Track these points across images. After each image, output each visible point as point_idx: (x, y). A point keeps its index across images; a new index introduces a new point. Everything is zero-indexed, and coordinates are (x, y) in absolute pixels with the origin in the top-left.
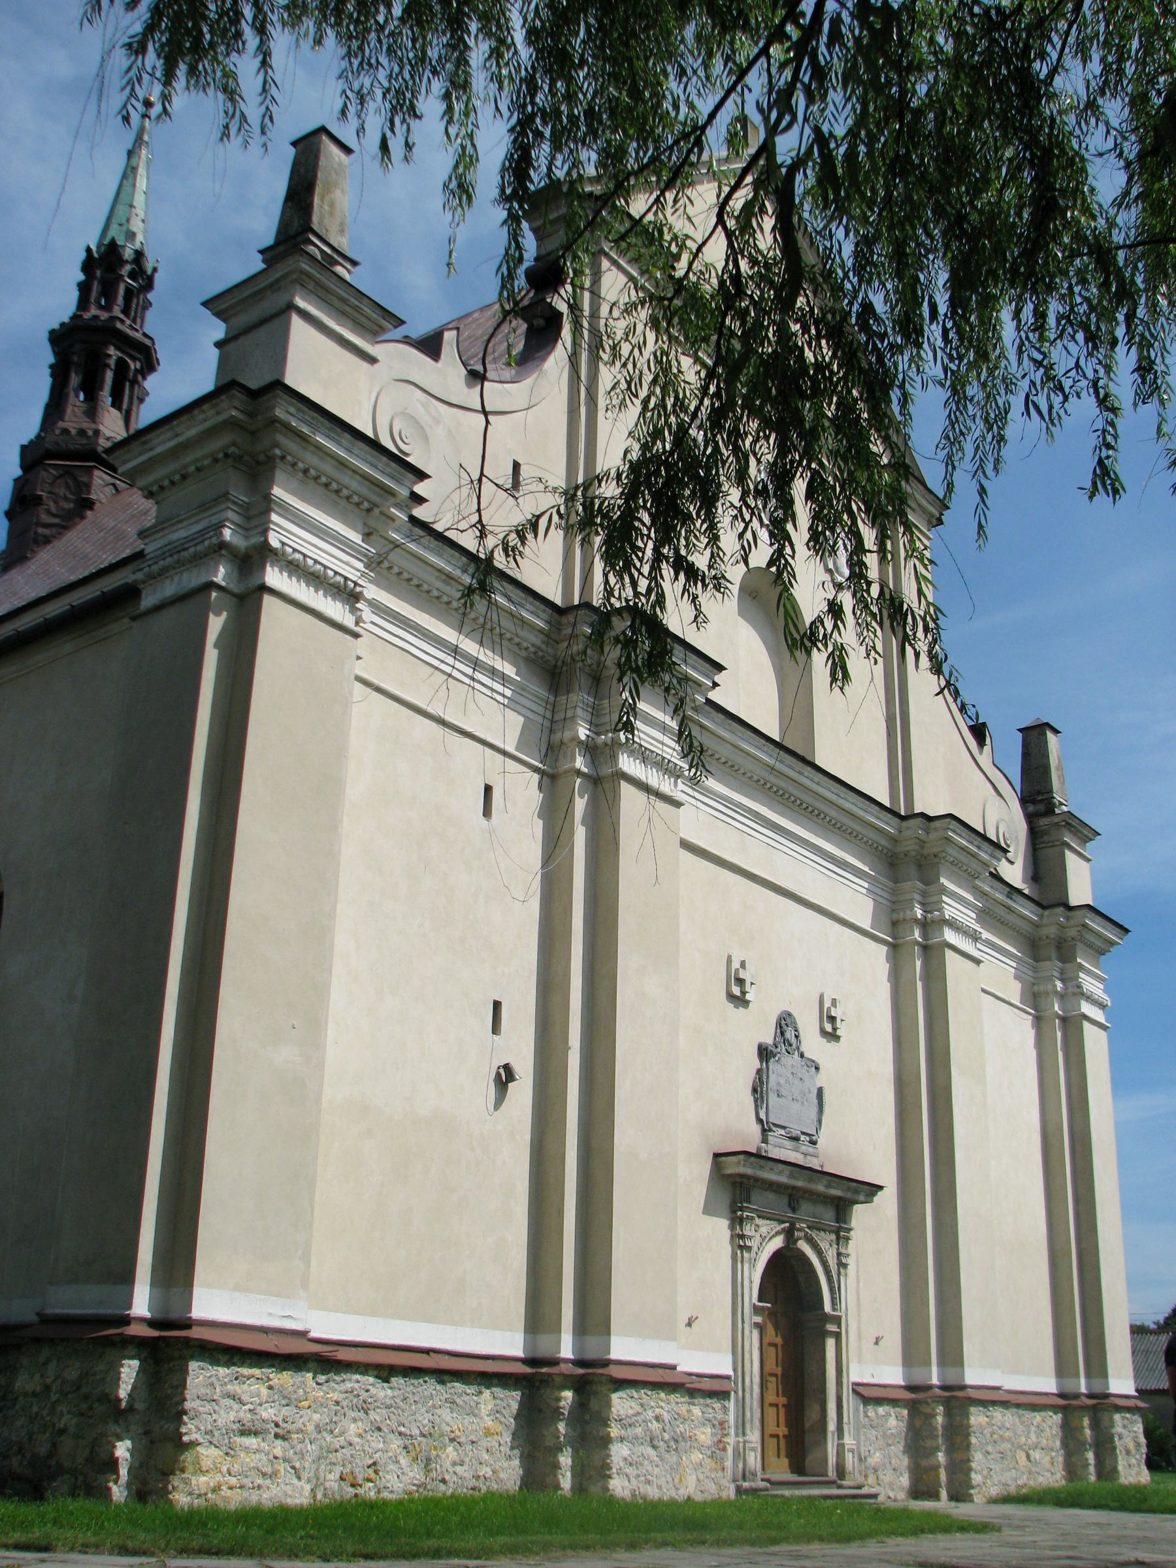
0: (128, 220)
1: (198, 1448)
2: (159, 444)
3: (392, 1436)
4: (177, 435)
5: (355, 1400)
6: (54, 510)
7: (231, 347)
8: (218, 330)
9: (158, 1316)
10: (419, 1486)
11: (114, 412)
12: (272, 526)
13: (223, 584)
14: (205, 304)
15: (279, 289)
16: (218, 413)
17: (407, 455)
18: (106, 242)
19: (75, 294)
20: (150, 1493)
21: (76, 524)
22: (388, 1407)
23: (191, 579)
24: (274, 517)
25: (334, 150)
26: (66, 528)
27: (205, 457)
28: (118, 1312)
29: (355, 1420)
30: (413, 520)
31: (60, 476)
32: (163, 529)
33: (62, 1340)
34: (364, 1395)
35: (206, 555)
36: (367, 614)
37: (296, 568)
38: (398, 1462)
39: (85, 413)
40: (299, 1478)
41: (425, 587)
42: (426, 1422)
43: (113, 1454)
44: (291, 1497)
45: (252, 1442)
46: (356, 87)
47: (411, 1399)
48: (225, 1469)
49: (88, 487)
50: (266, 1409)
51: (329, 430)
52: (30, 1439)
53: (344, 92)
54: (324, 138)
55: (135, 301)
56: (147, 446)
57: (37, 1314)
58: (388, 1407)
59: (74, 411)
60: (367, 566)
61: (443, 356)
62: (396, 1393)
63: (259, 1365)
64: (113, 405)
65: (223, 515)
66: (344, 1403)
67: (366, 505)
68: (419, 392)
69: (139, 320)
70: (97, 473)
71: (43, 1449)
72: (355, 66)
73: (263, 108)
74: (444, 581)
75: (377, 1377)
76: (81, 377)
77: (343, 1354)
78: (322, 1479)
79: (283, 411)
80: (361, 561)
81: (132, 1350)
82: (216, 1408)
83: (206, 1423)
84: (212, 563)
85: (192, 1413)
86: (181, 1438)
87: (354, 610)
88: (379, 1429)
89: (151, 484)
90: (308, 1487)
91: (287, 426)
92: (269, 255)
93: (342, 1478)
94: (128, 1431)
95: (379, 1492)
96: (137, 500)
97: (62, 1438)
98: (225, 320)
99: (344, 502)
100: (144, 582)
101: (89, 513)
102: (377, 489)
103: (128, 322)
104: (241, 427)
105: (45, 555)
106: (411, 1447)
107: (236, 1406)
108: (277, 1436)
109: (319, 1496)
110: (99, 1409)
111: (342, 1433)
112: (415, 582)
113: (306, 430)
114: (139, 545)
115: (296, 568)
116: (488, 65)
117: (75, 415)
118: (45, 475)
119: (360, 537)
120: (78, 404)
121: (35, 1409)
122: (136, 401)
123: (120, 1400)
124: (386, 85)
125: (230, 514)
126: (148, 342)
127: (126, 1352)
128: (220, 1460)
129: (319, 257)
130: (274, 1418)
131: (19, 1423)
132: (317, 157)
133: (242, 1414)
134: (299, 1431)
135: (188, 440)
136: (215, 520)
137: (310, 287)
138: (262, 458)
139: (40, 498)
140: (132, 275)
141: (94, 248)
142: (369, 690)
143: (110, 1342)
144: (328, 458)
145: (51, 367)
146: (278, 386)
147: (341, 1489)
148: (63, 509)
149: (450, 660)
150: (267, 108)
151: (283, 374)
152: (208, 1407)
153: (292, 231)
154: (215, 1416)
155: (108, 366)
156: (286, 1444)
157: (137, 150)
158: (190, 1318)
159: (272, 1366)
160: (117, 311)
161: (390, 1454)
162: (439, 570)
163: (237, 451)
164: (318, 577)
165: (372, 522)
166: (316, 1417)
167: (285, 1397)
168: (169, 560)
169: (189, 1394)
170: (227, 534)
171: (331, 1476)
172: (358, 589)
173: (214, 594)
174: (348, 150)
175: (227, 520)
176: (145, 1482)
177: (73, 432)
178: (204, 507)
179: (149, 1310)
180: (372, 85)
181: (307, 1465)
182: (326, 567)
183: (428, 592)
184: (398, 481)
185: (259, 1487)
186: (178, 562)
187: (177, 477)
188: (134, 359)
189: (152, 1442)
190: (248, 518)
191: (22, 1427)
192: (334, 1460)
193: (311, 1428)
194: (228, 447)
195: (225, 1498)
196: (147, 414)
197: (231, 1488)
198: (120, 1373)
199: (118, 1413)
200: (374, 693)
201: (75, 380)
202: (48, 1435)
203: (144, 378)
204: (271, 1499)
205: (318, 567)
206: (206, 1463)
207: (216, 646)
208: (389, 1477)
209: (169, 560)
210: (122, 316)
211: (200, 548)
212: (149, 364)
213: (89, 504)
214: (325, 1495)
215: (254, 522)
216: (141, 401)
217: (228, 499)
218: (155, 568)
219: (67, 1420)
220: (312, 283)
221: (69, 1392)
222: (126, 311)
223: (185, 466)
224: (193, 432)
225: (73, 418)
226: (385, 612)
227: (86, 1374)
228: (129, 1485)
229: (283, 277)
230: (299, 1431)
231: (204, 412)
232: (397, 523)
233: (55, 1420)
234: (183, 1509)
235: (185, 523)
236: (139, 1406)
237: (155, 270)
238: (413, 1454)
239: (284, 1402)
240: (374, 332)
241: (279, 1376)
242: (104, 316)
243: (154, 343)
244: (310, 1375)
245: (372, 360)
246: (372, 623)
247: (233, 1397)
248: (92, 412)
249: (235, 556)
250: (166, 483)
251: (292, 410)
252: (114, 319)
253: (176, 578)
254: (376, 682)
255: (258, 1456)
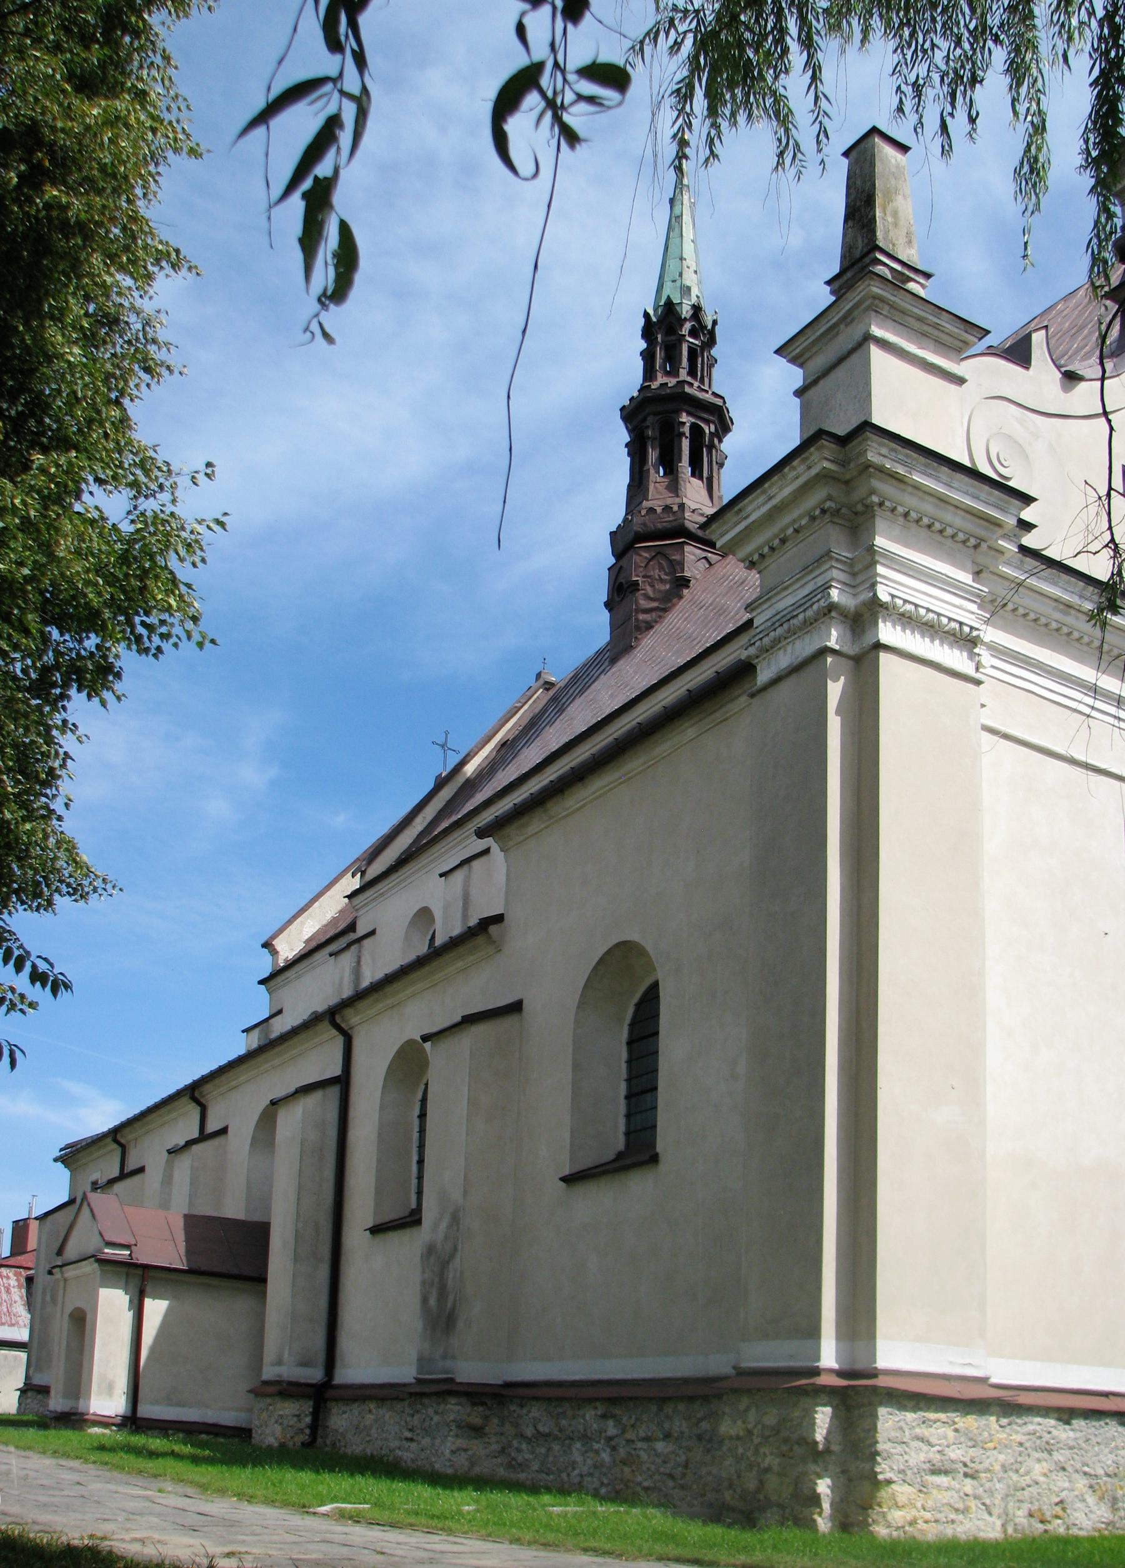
0: (681, 275)
1: (893, 1486)
2: (754, 510)
3: (1076, 1476)
4: (770, 498)
5: (1038, 1442)
6: (651, 595)
7: (810, 393)
8: (796, 376)
9: (846, 1367)
10: (1108, 1524)
11: (695, 482)
12: (879, 579)
13: (837, 647)
14: (778, 352)
15: (852, 321)
16: (810, 468)
17: (1008, 479)
18: (662, 303)
19: (639, 364)
20: (852, 1525)
21: (674, 605)
22: (1071, 1448)
23: (804, 647)
24: (880, 569)
25: (888, 151)
26: (665, 610)
27: (801, 517)
28: (809, 1364)
29: (1039, 1460)
30: (1023, 549)
31: (653, 558)
32: (768, 599)
33: (759, 1390)
34: (1047, 1437)
35: (816, 620)
36: (986, 658)
37: (908, 620)
38: (1084, 1501)
39: (667, 488)
40: (990, 1514)
41: (1043, 620)
42: (1109, 1462)
43: (815, 1491)
44: (983, 1531)
45: (943, 1480)
46: (912, 78)
47: (1094, 1440)
48: (919, 1505)
49: (681, 564)
50: (953, 1450)
51: (926, 465)
52: (739, 1477)
53: (899, 88)
54: (877, 140)
55: (700, 360)
56: (744, 514)
57: (734, 1368)
58: (1071, 1448)
59: (655, 487)
60: (980, 607)
61: (1033, 363)
62: (1078, 1434)
63: (944, 1410)
64: (693, 475)
65: (828, 576)
66: (1028, 1445)
67: (973, 541)
68: (1013, 407)
69: (706, 380)
70: (687, 548)
71: (752, 1485)
72: (909, 57)
73: (817, 125)
74: (1061, 611)
75: (1059, 1419)
76: (658, 451)
77: (1024, 1399)
78: (1011, 1516)
79: (875, 453)
80: (975, 602)
81: (824, 1398)
82: (907, 1449)
83: (898, 1463)
84: (823, 627)
85: (884, 1455)
86: (876, 1477)
87: (972, 655)
88: (1064, 1469)
89: (751, 554)
90: (999, 1523)
91: (881, 470)
92: (837, 284)
93: (1031, 1515)
94: (827, 1471)
95: (1068, 1528)
96: (733, 569)
97: (768, 1476)
98: (801, 366)
99: (949, 542)
100: (757, 657)
101: (685, 591)
102: (982, 522)
103: (696, 384)
104: (834, 478)
105: (648, 643)
106: (1097, 1487)
107: (925, 1448)
108: (966, 1475)
109: (1010, 1531)
110: (798, 1450)
111: (1028, 1473)
112: (1032, 616)
113: (901, 470)
114: (748, 616)
115: (908, 620)
116: (1055, 18)
117: (659, 493)
118: (638, 559)
119: (970, 577)
120: (659, 479)
121: (740, 1450)
122: (715, 467)
123: (816, 1443)
124: (944, 67)
125: (835, 573)
126: (719, 402)
127: (818, 1400)
128: (914, 1496)
129: (890, 277)
130: (963, 1459)
131: (727, 1463)
132: (872, 165)
133: (931, 1455)
134: (987, 1470)
135: (782, 502)
136: (820, 581)
137: (885, 313)
138: (860, 508)
139: (636, 583)
140: (693, 333)
141: (651, 312)
142: (996, 738)
143: (803, 1391)
144: (927, 497)
145: (627, 445)
146: (867, 426)
147: (1030, 1525)
148: (660, 591)
149: (1090, 701)
150: (821, 123)
151: (870, 414)
152: (899, 1449)
153: (857, 254)
154: (906, 1457)
155: (683, 434)
156: (975, 1482)
157: (679, 197)
158: (876, 1368)
159: (956, 1410)
160: (683, 375)
161: (1076, 1493)
162: (1056, 600)
163: (833, 505)
164: (932, 626)
165: (981, 559)
166: (1002, 1457)
167: (971, 1439)
168: (779, 631)
169: (881, 1436)
170: (835, 594)
171: (1019, 1513)
172: (975, 633)
173: (829, 660)
174: (904, 148)
175: (832, 579)
176: (846, 1516)
177: (659, 510)
178: (807, 569)
179: (837, 1361)
180: (929, 71)
181: (997, 1502)
182: (939, 615)
183: (1046, 625)
184: (1004, 510)
185: (953, 1522)
186: (789, 631)
187: (776, 542)
188: (708, 422)
189: (850, 1480)
190: (854, 575)
191: (730, 1465)
192: (1022, 1498)
193: (997, 1468)
194: (824, 501)
195: (921, 1531)
196: (731, 482)
197: (926, 1522)
198: (815, 1418)
199: (814, 1453)
200: (1001, 740)
201: (653, 455)
202: (754, 1473)
203: (720, 441)
204: (965, 1533)
205: (931, 615)
206: (901, 1499)
207: (837, 713)
208: (1076, 1514)
209: (779, 631)
210: (689, 379)
211: (809, 613)
212: (724, 426)
213: (684, 583)
214: (1015, 1530)
215: (860, 579)
216: (721, 465)
217: (831, 558)
218: (766, 640)
219: (770, 1460)
220: (887, 307)
221: (770, 1436)
222: (692, 372)
223: (783, 530)
224: (787, 491)
225: (657, 495)
226: (1004, 653)
227: (784, 1419)
228: (832, 1517)
229: (856, 306)
230: (987, 1470)
231: (794, 468)
232: (1007, 555)
233: (760, 1460)
234: (885, 1541)
235: (790, 591)
236: (835, 1448)
237: (715, 323)
238: (1099, 1493)
239: (970, 1444)
240: (958, 350)
241: (964, 1419)
242: (672, 382)
243: (725, 403)
244: (993, 1419)
245: (960, 381)
246: (993, 667)
247: (922, 1439)
248: (674, 487)
249: (845, 616)
250: (766, 550)
251: (884, 451)
252: (683, 383)
253: (789, 648)
254: (1003, 729)
255: (949, 1493)
